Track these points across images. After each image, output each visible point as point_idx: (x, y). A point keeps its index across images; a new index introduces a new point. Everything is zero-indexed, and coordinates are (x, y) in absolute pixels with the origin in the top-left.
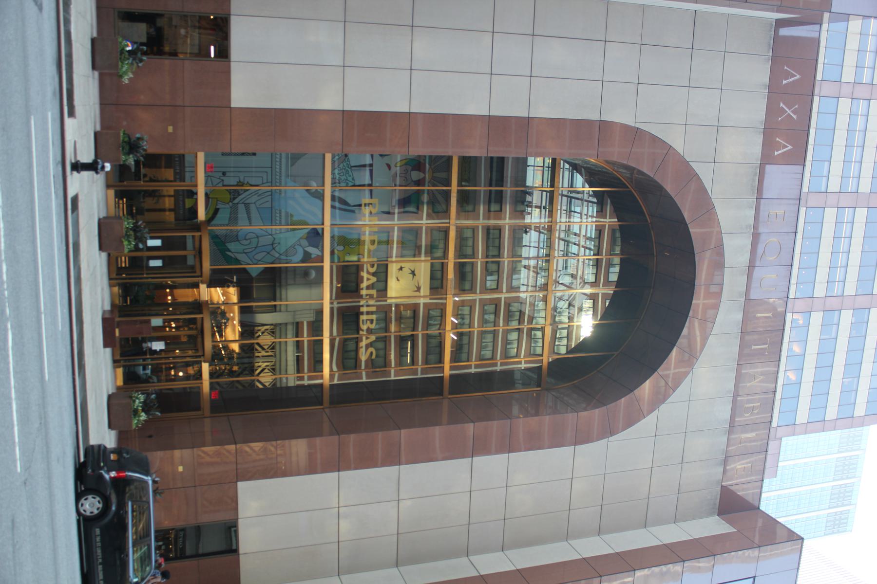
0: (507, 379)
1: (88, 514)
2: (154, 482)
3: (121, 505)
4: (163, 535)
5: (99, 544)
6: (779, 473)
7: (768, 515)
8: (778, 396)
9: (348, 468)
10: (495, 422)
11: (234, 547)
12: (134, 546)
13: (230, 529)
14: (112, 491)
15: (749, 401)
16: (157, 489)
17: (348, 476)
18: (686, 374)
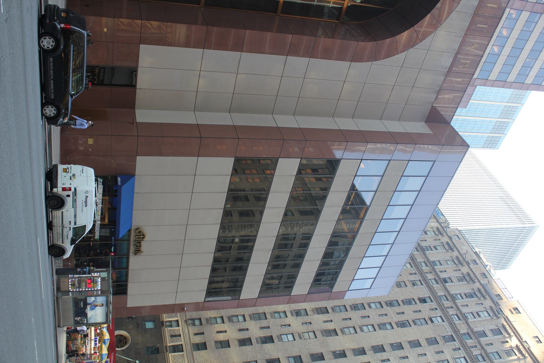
0: (319, 11)
1: (46, 48)
2: (88, 35)
3: (67, 46)
4: (91, 69)
5: (52, 68)
6: (468, 106)
7: (454, 129)
8: (483, 60)
9: (210, 48)
10: (306, 37)
11: (134, 84)
12: (73, 72)
13: (133, 73)
14: (62, 36)
15: (464, 59)
16: (90, 40)
17: (209, 52)
18: (431, 33)
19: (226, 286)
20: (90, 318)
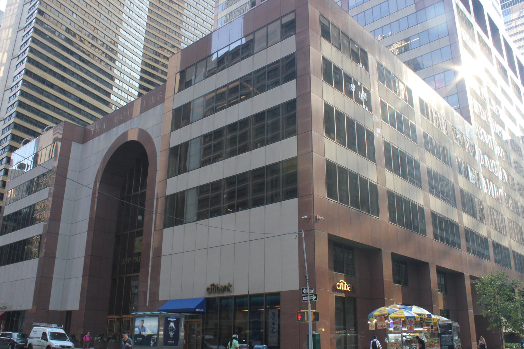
19: (517, 17)
20: (153, 332)
